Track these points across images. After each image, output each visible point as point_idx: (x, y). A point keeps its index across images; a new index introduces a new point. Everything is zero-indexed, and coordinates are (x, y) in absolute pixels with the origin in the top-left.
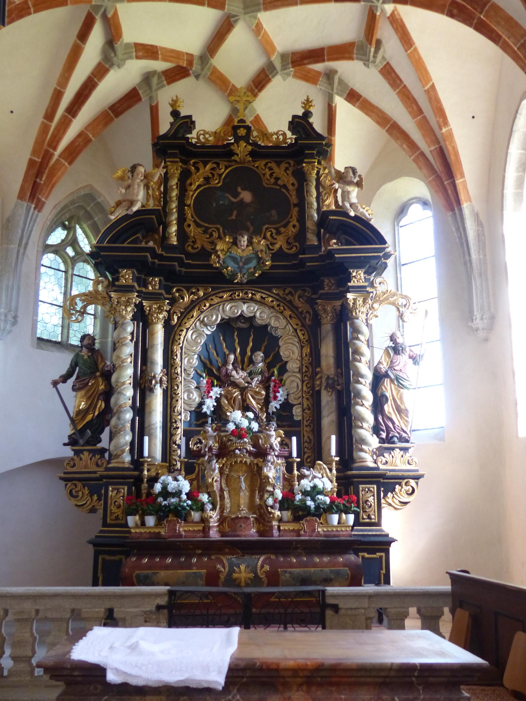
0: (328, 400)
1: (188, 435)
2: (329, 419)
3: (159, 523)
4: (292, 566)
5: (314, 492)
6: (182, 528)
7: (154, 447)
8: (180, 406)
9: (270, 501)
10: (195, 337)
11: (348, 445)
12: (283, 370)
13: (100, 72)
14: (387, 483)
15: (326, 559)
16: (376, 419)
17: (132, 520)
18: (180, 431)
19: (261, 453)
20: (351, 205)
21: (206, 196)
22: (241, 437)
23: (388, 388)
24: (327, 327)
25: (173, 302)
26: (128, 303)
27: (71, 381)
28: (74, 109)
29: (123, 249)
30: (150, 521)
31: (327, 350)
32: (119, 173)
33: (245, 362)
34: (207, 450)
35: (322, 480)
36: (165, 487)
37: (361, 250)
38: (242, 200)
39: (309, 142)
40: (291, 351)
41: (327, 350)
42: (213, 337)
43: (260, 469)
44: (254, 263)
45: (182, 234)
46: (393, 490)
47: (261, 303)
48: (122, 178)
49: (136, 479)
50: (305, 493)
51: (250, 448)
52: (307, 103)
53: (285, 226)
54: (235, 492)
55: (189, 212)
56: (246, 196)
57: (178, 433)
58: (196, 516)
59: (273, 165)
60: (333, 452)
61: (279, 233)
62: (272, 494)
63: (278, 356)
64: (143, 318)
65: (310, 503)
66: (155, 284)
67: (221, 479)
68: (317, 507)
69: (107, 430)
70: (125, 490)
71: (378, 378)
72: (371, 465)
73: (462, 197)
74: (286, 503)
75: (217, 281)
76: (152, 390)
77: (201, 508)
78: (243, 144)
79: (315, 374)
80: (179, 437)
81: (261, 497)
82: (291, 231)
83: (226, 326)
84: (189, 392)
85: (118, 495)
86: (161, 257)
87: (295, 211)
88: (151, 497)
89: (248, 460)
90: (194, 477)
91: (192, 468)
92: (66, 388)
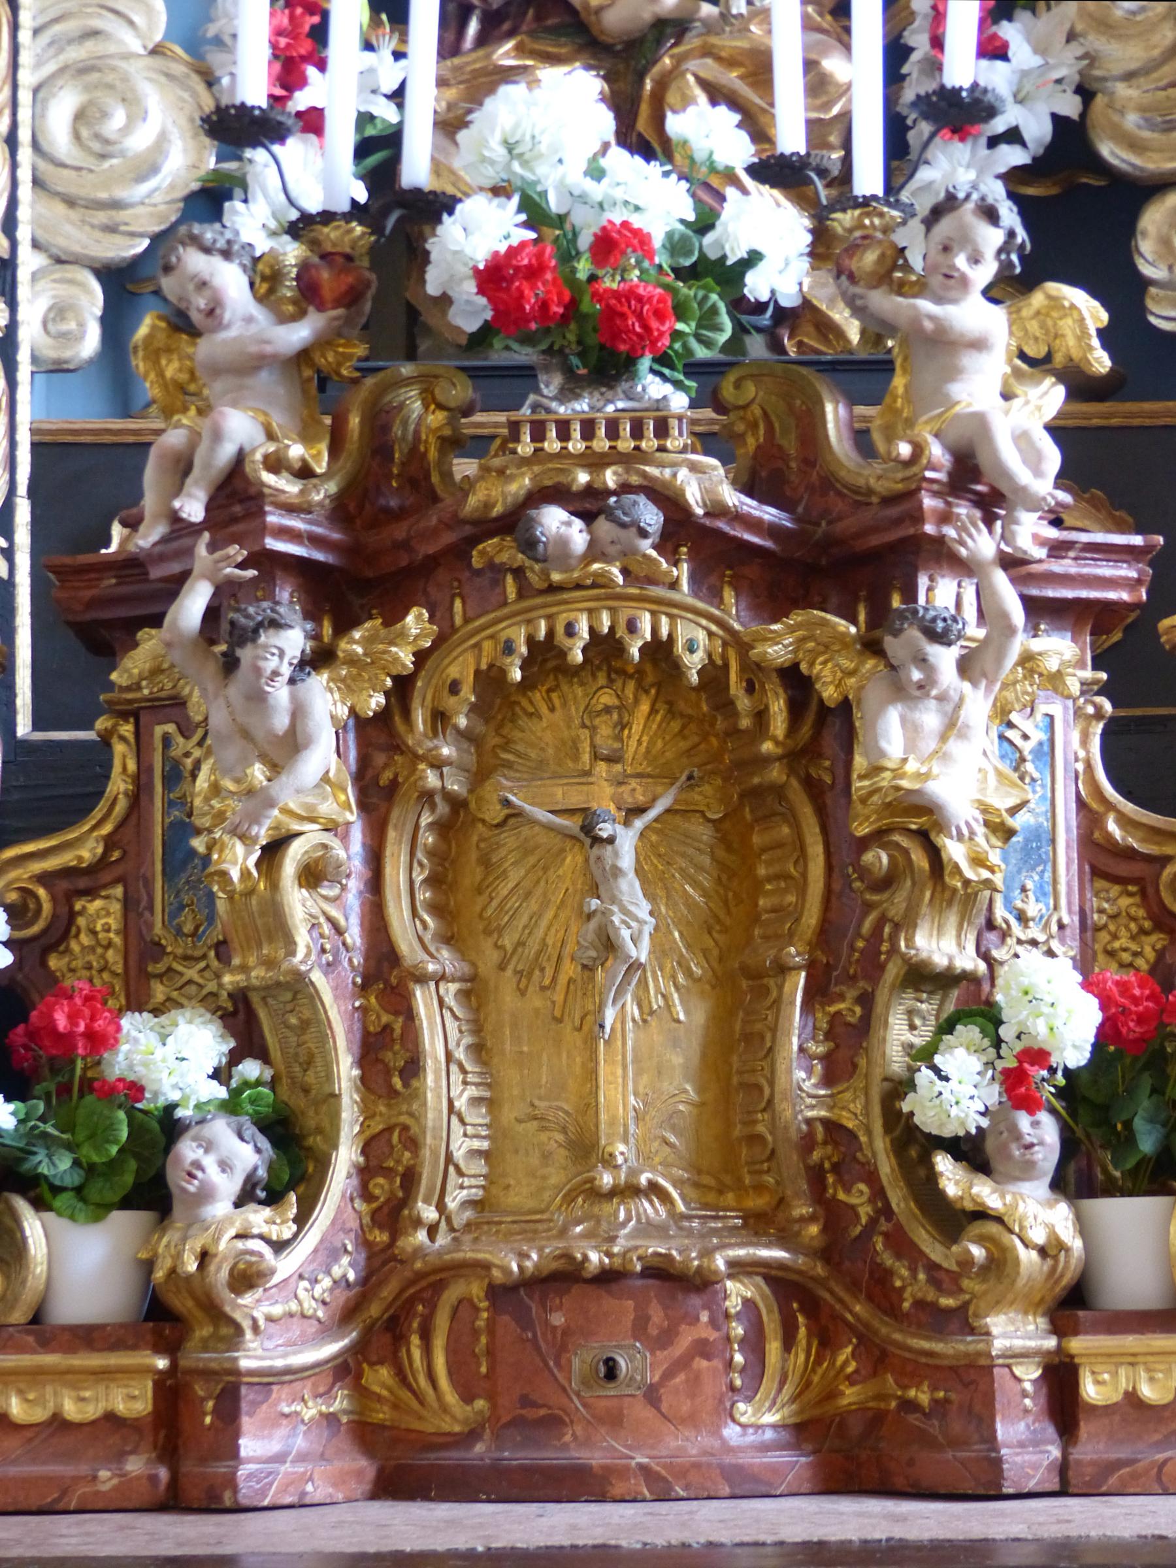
34: (193, 509)
67: (375, 858)
90: (89, 852)
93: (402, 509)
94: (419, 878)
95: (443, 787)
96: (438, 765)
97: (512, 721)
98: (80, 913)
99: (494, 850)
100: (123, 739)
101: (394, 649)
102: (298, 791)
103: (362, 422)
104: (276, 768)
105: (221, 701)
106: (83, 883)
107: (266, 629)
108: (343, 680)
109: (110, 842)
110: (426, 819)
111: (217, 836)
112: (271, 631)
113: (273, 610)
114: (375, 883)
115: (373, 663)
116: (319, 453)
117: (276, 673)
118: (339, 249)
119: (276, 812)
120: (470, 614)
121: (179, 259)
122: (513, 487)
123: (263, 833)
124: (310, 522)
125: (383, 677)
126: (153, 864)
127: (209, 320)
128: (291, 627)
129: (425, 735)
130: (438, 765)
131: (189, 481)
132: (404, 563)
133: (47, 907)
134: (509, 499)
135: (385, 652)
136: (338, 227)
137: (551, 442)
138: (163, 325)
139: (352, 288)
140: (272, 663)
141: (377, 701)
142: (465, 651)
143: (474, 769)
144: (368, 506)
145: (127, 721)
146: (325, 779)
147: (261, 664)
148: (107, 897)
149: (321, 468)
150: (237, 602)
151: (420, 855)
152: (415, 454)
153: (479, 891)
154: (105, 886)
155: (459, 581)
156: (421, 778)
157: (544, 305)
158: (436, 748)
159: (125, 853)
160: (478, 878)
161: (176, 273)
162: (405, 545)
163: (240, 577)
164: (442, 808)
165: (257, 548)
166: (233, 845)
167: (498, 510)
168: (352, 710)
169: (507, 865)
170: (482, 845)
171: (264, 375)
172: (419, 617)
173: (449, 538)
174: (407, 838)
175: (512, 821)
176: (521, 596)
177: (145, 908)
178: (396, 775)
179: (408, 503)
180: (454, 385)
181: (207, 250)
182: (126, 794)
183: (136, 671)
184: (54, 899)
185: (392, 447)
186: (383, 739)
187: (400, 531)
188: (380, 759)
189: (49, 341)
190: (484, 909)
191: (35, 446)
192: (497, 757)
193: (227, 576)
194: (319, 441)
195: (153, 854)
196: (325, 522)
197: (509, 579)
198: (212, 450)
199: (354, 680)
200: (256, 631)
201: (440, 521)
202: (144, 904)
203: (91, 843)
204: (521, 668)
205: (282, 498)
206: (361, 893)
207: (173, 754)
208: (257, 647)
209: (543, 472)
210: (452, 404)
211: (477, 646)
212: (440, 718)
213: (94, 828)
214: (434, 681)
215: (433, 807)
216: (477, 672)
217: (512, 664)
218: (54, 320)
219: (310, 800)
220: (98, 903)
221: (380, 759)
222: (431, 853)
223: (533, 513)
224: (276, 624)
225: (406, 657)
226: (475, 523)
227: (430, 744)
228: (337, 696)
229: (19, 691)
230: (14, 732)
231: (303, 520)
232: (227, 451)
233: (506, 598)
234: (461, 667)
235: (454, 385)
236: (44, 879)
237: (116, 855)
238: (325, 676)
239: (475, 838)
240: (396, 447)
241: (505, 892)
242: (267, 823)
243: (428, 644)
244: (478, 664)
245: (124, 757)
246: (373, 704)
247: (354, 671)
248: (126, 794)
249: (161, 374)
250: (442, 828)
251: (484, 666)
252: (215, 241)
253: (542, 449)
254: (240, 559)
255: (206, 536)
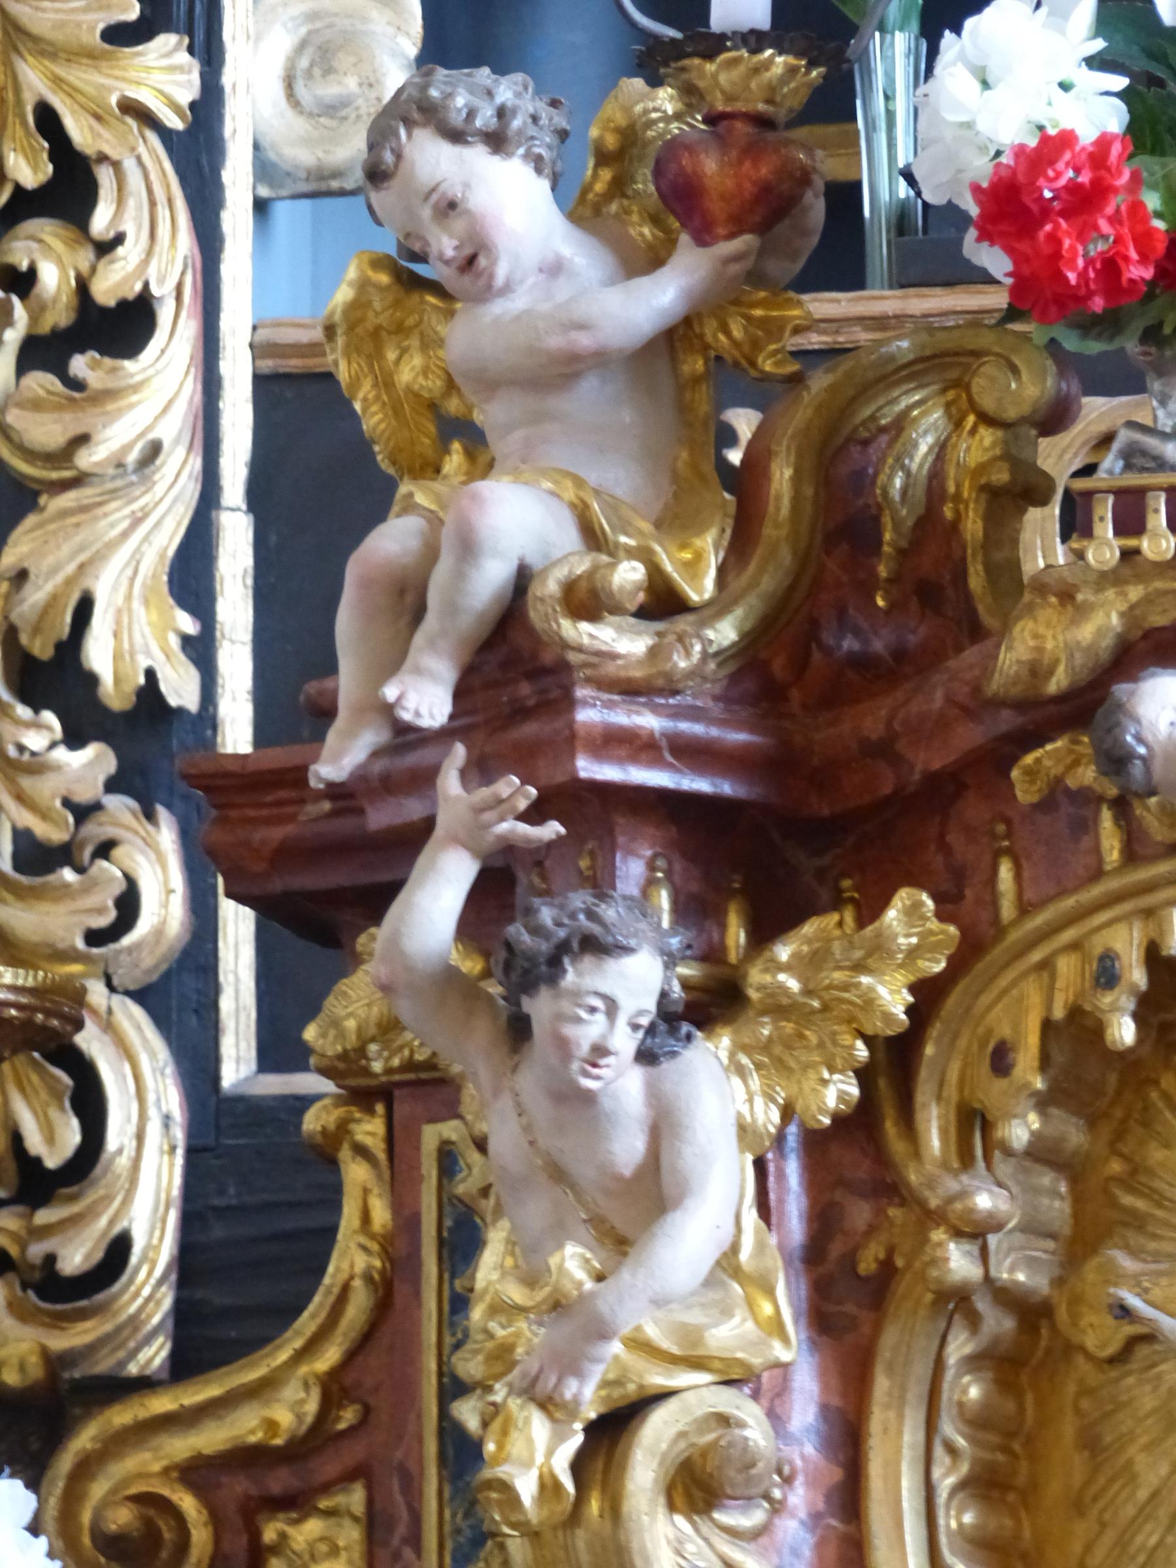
34: (427, 699)
57: (115, 438)
67: (847, 1438)
80: (168, 533)
90: (289, 1411)
93: (900, 654)
94: (945, 1482)
95: (987, 1277)
96: (976, 1232)
97: (1146, 1124)
98: (276, 1549)
99: (1107, 1415)
100: (361, 1151)
101: (865, 980)
102: (659, 1303)
103: (796, 480)
104: (618, 1242)
105: (505, 1103)
106: (279, 1481)
107: (575, 958)
108: (766, 1047)
109: (335, 1388)
110: (959, 1346)
111: (498, 1398)
112: (588, 961)
113: (591, 915)
114: (848, 1498)
115: (825, 1008)
116: (699, 556)
117: (600, 1051)
118: (740, 106)
119: (616, 1347)
120: (1029, 895)
121: (399, 156)
122: (1086, 632)
123: (588, 1396)
124: (678, 713)
125: (846, 1039)
126: (420, 1440)
127: (466, 279)
128: (627, 950)
129: (945, 1165)
130: (976, 1232)
131: (419, 638)
132: (887, 788)
133: (201, 1536)
134: (1079, 659)
135: (846, 987)
136: (736, 61)
137: (1156, 536)
138: (384, 278)
139: (765, 190)
140: (591, 1030)
141: (837, 1092)
142: (1024, 975)
143: (1067, 1231)
144: (817, 655)
145: (371, 1112)
146: (728, 1263)
147: (569, 1030)
148: (330, 1513)
149: (702, 588)
150: (544, 877)
151: (949, 1428)
152: (932, 524)
153: (1079, 1507)
154: (326, 1488)
155: (1008, 822)
156: (934, 1262)
157: (1110, 266)
158: (964, 1194)
159: (367, 1411)
160: (1078, 1479)
161: (395, 183)
162: (883, 750)
163: (527, 839)
164: (998, 1323)
165: (560, 778)
166: (527, 1421)
167: (1057, 683)
168: (787, 1112)
169: (1132, 1450)
170: (1085, 1404)
171: (589, 385)
172: (913, 912)
173: (969, 736)
174: (917, 1391)
175: (1143, 1352)
176: (1132, 856)
177: (406, 1541)
178: (891, 1251)
179: (912, 640)
180: (1015, 370)
181: (456, 136)
182: (368, 1278)
183: (351, 1024)
184: (216, 1519)
185: (877, 520)
186: (862, 1170)
187: (871, 719)
188: (859, 1213)
189: (300, 125)
190: (1088, 1548)
191: (262, 382)
192: (1114, 1203)
193: (501, 838)
194: (701, 531)
195: (419, 1417)
196: (716, 709)
197: (1106, 819)
198: (460, 576)
199: (789, 1047)
200: (555, 963)
201: (950, 701)
202: (401, 1530)
203: (292, 1391)
204: (1137, 1017)
205: (610, 669)
206: (816, 1517)
207: (460, 1189)
208: (559, 995)
209: (1147, 600)
210: (1012, 413)
211: (1047, 965)
212: (974, 1125)
213: (300, 1356)
214: (962, 1043)
215: (974, 1321)
216: (1048, 1026)
217: (1115, 1008)
218: (309, 74)
219: (694, 1317)
220: (313, 1527)
221: (859, 1213)
222: (978, 1422)
223: (1121, 689)
224: (596, 946)
225: (893, 999)
226: (1020, 705)
227: (951, 1185)
228: (755, 1082)
229: (226, 977)
230: (216, 1078)
231: (656, 710)
232: (491, 577)
233: (1100, 860)
234: (1021, 1011)
235: (1015, 370)
236: (196, 1473)
237: (348, 1417)
238: (725, 1041)
239: (1071, 1388)
240: (887, 520)
241: (1130, 1511)
242: (597, 1373)
243: (939, 967)
244: (1049, 1003)
245: (366, 1192)
246: (831, 1099)
247: (789, 1027)
248: (368, 1278)
249: (386, 382)
250: (1003, 1365)
251: (1059, 1013)
252: (471, 114)
253: (1137, 551)
254: (522, 805)
255: (460, 751)
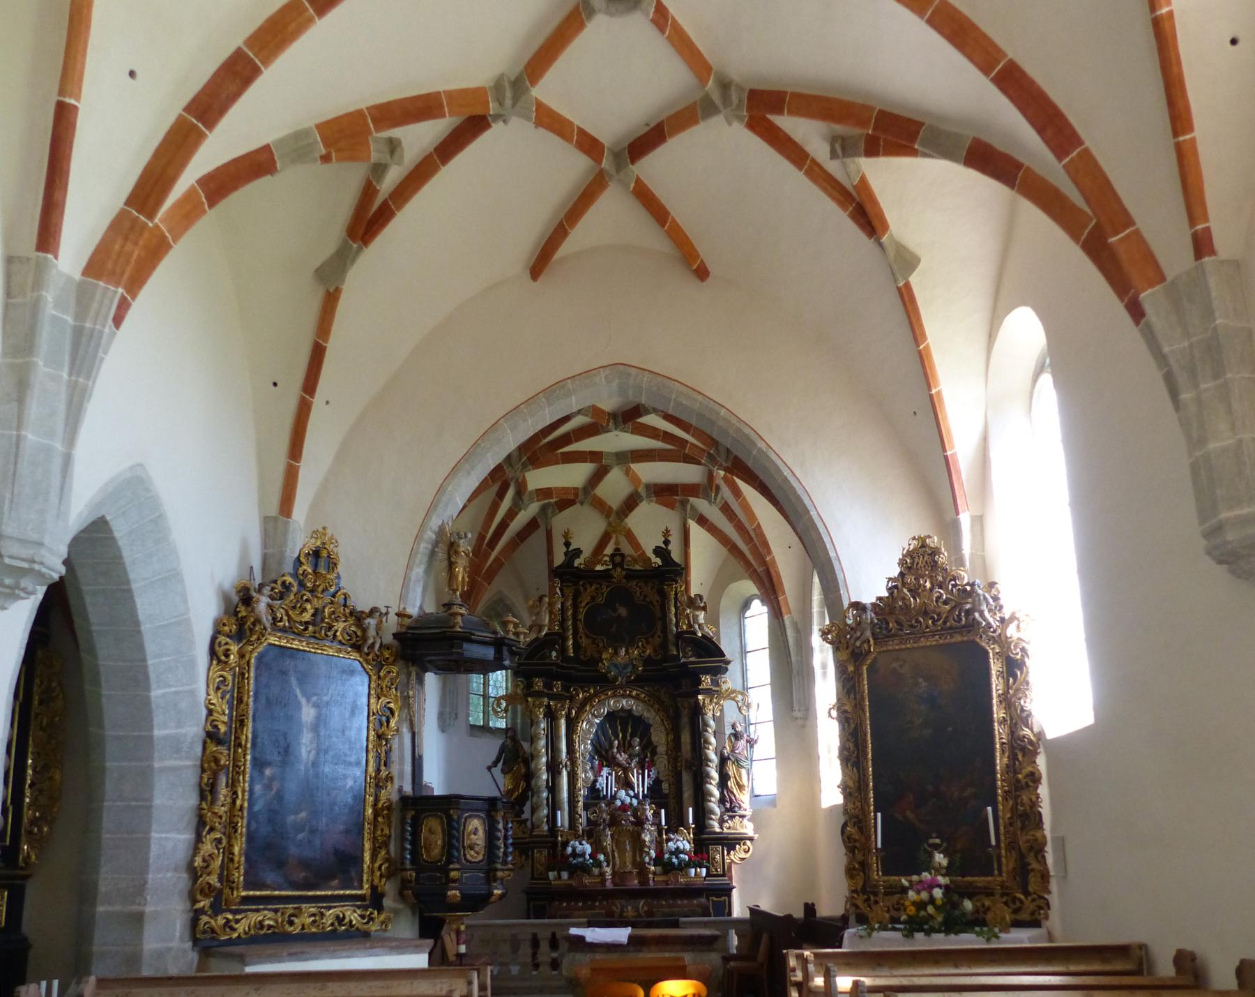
0: (686, 778)
1: (586, 807)
2: (687, 794)
3: (570, 877)
4: (662, 906)
5: (678, 851)
6: (586, 881)
7: (562, 818)
8: (580, 784)
9: (647, 859)
10: (588, 726)
11: (702, 814)
12: (654, 753)
13: (511, 514)
14: (731, 842)
15: (685, 902)
16: (722, 793)
17: (552, 875)
18: (581, 804)
19: (640, 822)
20: (700, 625)
21: (593, 612)
22: (625, 811)
23: (731, 769)
24: (685, 720)
25: (572, 698)
26: (540, 706)
27: (500, 765)
28: (492, 545)
29: (536, 665)
30: (565, 875)
31: (686, 738)
32: (531, 603)
33: (625, 746)
35: (683, 843)
36: (574, 849)
37: (710, 662)
38: (619, 616)
39: (670, 571)
40: (659, 737)
41: (686, 738)
42: (601, 725)
43: (639, 835)
44: (629, 669)
45: (576, 646)
46: (734, 849)
47: (637, 698)
48: (532, 607)
49: (552, 843)
50: (671, 853)
51: (632, 819)
52: (667, 533)
53: (652, 636)
54: (622, 852)
55: (581, 627)
56: (623, 611)
58: (596, 871)
59: (641, 584)
60: (691, 821)
61: (648, 642)
62: (648, 854)
63: (650, 743)
64: (551, 716)
65: (675, 860)
66: (558, 686)
68: (680, 863)
69: (528, 804)
70: (545, 852)
71: (723, 761)
72: (718, 830)
73: (784, 610)
74: (658, 860)
75: (604, 683)
76: (560, 773)
77: (599, 864)
78: (619, 570)
79: (676, 759)
81: (641, 856)
82: (657, 641)
83: (611, 717)
84: (585, 771)
85: (541, 855)
86: (562, 667)
87: (659, 623)
88: (566, 857)
89: (630, 828)
91: (592, 834)
92: (497, 771)
